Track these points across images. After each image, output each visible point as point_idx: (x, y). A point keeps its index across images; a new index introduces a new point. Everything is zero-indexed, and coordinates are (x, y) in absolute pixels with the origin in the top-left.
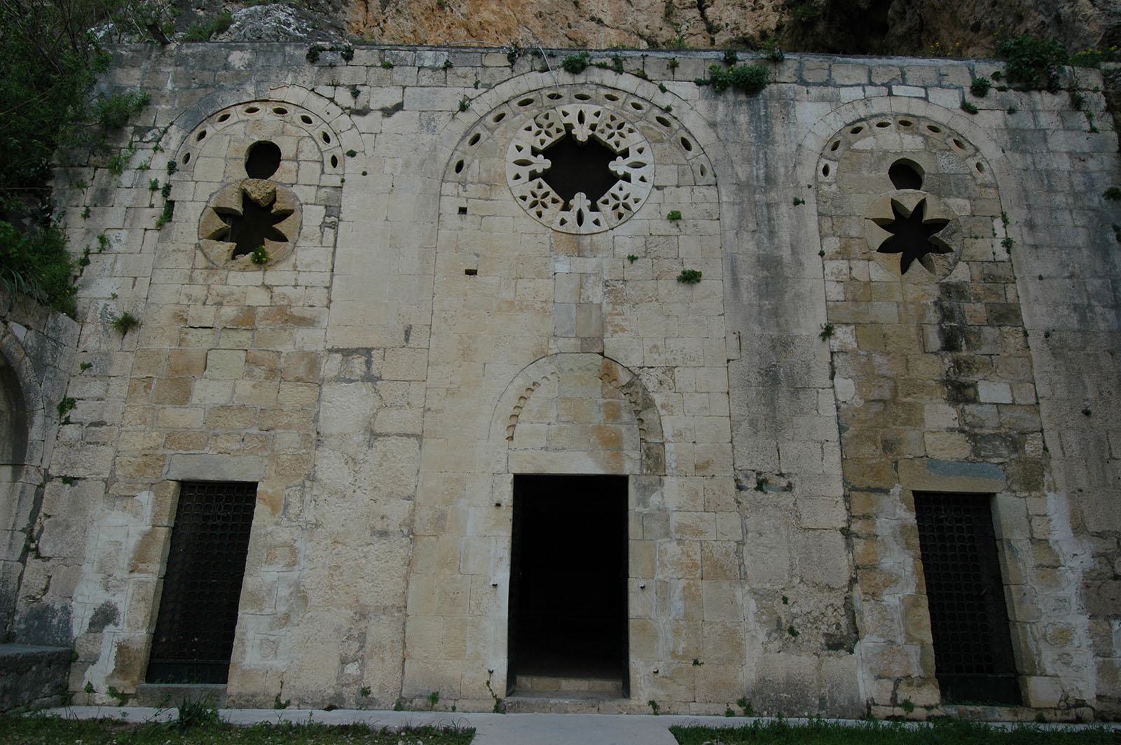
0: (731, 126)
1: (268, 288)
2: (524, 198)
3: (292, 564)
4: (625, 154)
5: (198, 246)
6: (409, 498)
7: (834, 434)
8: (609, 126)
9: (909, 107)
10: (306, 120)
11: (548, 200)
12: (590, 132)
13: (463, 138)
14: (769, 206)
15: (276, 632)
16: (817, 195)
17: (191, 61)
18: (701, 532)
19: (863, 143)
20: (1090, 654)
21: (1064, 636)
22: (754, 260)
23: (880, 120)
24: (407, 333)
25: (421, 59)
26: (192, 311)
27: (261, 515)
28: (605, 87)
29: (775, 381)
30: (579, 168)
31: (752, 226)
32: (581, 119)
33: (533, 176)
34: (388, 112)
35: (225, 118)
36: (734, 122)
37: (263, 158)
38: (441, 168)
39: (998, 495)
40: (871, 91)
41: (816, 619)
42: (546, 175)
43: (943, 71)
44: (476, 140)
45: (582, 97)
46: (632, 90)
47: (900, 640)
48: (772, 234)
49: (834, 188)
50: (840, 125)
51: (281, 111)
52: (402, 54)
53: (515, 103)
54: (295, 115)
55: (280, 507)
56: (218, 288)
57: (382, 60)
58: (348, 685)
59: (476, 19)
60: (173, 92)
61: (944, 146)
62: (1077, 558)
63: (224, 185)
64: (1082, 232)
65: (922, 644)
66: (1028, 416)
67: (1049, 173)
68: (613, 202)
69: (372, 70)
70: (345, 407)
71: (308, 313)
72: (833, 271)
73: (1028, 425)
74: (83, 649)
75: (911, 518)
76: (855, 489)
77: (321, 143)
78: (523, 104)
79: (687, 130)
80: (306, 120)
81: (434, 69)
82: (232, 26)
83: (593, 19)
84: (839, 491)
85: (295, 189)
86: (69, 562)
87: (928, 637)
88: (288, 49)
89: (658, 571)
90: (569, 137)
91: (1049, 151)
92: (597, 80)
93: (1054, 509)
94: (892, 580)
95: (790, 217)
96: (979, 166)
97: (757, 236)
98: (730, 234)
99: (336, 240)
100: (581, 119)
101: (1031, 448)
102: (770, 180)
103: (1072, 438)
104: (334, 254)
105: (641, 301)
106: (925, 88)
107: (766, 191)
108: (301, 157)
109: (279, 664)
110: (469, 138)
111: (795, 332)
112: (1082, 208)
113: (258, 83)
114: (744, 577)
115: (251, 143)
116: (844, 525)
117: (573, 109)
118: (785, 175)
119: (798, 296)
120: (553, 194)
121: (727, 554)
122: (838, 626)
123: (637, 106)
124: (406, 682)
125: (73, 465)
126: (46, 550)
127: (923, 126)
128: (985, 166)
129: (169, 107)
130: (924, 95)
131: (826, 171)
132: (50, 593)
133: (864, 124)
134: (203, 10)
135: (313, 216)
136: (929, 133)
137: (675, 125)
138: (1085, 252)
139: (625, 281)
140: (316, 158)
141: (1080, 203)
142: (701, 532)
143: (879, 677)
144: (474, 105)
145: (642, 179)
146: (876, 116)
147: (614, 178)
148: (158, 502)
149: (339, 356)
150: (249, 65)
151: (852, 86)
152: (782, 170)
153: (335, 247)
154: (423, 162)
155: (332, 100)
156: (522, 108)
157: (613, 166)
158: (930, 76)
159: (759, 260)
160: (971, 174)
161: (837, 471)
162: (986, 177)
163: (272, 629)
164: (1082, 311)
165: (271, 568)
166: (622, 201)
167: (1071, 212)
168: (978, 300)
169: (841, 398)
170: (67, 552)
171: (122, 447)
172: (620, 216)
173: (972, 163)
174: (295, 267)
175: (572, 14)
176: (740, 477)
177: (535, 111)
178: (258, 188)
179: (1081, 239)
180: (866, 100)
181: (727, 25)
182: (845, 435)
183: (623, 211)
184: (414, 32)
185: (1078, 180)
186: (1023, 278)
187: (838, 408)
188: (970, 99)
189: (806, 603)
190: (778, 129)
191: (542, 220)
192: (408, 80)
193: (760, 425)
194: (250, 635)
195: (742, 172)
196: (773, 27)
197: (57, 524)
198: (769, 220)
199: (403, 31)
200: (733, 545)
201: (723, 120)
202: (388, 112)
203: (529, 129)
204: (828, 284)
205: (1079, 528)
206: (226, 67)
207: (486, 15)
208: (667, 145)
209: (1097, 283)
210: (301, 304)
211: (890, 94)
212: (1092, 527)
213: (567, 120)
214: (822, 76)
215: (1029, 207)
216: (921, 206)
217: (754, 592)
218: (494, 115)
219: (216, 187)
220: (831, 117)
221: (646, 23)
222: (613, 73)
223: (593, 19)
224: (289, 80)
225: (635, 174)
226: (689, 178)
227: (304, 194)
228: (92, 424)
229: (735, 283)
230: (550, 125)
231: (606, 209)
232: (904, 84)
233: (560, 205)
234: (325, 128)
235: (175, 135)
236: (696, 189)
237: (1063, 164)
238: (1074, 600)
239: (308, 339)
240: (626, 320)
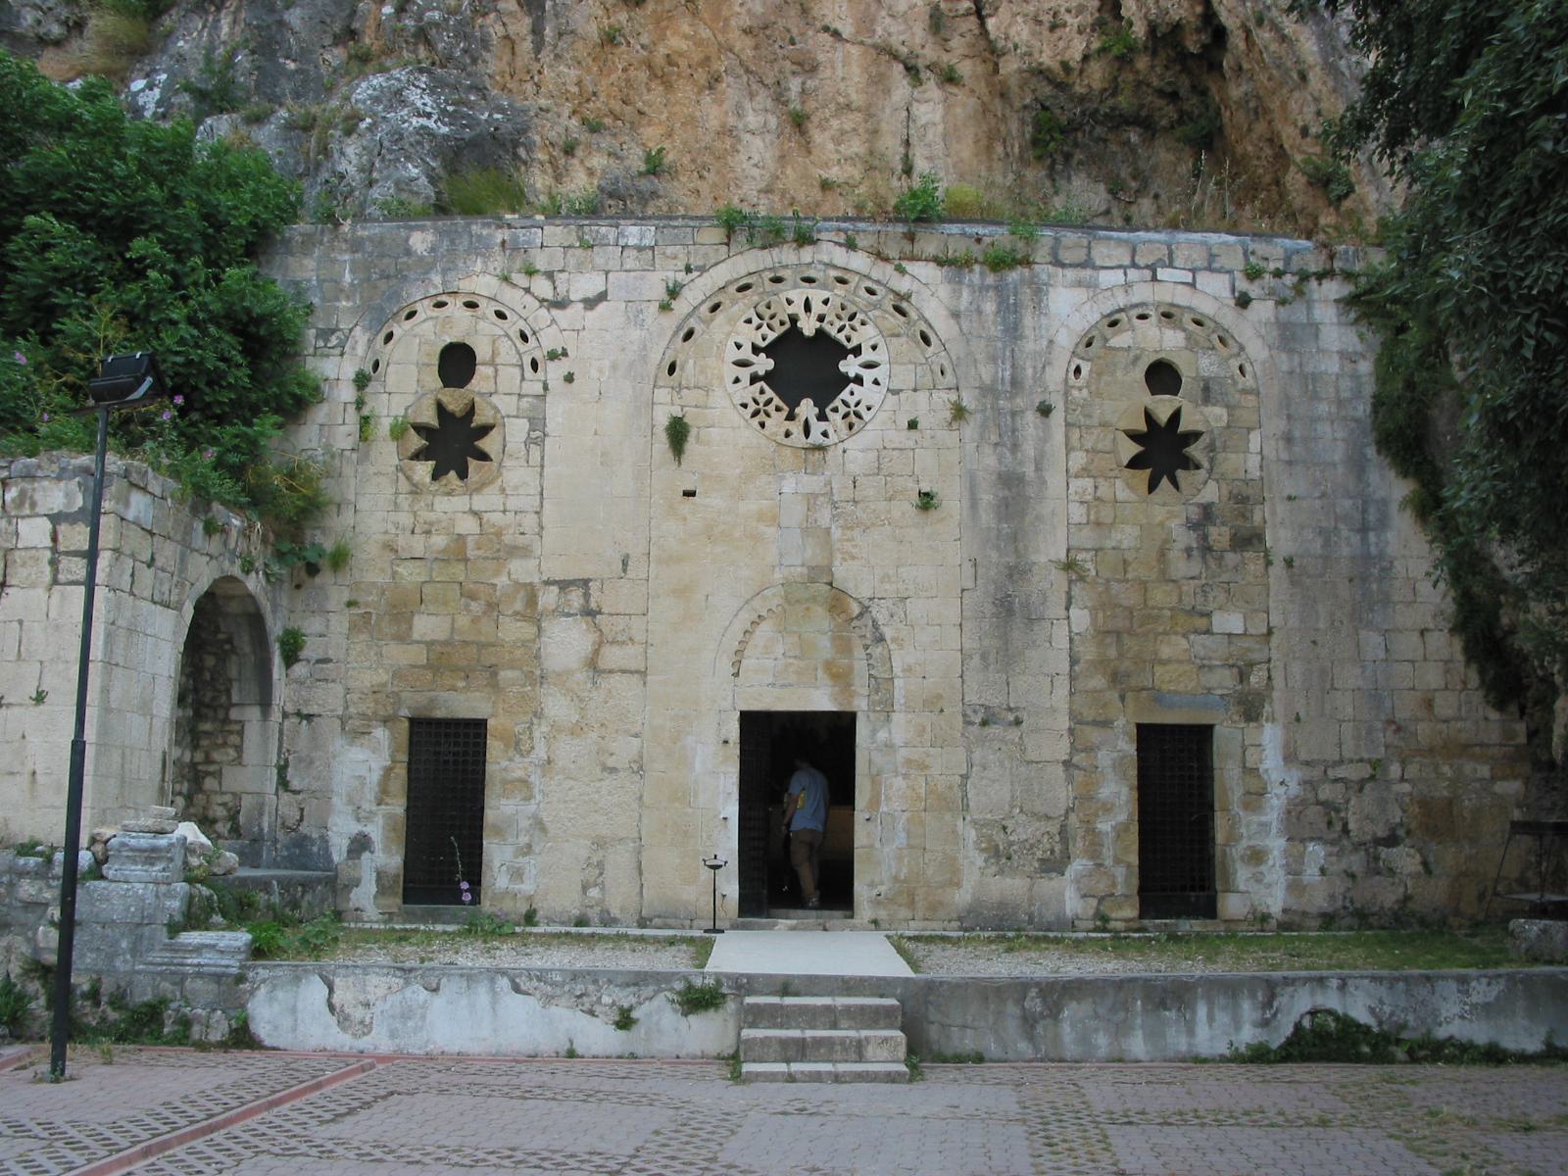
0: (975, 316)
1: (475, 513)
2: (745, 406)
3: (528, 798)
4: (857, 351)
5: (399, 469)
6: (636, 736)
7: (1065, 667)
8: (839, 317)
9: (1174, 295)
10: (501, 315)
11: (771, 408)
12: (818, 325)
13: (676, 333)
14: (1014, 414)
15: (520, 859)
16: (1066, 402)
17: (369, 247)
18: (927, 767)
19: (1120, 340)
20: (1282, 873)
21: (1257, 856)
22: (994, 477)
23: (1140, 311)
24: (625, 564)
25: (624, 236)
26: (401, 542)
27: (494, 748)
28: (835, 267)
29: (1010, 612)
30: (806, 369)
31: (994, 438)
32: (808, 307)
33: (754, 379)
34: (591, 303)
35: (411, 315)
36: (979, 312)
37: (457, 363)
38: (652, 369)
39: (1217, 729)
40: (1133, 274)
41: (1032, 846)
42: (768, 378)
43: (1215, 251)
44: (689, 335)
45: (809, 280)
46: (866, 271)
47: (1108, 862)
48: (1015, 447)
49: (1085, 392)
50: (1097, 317)
51: (471, 305)
52: (603, 230)
53: (732, 289)
54: (487, 309)
55: (515, 744)
56: (425, 515)
57: (581, 239)
58: (592, 907)
59: (662, 50)
60: (352, 285)
61: (1207, 344)
62: (1282, 783)
63: (420, 398)
64: (1341, 445)
65: (1129, 866)
66: (1257, 646)
67: (1315, 377)
68: (843, 410)
69: (570, 252)
70: (565, 643)
71: (521, 540)
72: (1079, 492)
73: (1256, 656)
74: (345, 874)
75: (1131, 749)
76: (1080, 723)
77: (519, 342)
78: (741, 289)
79: (926, 321)
80: (501, 315)
81: (640, 249)
82: (363, 125)
83: (826, 29)
84: (1064, 723)
85: (494, 399)
86: (319, 795)
87: (1134, 859)
88: (474, 227)
89: (883, 804)
90: (794, 330)
91: (1319, 350)
92: (826, 259)
93: (1270, 737)
94: (1107, 808)
95: (1036, 428)
96: (1241, 369)
97: (999, 448)
98: (970, 447)
99: (542, 458)
100: (808, 307)
101: (1256, 679)
102: (1016, 383)
103: (1297, 669)
104: (541, 475)
105: (873, 524)
106: (1194, 271)
107: (1012, 397)
108: (498, 360)
109: (527, 887)
110: (682, 334)
111: (1033, 558)
112: (1345, 418)
113: (444, 272)
114: (966, 808)
115: (443, 345)
116: (1066, 757)
117: (798, 295)
118: (1034, 378)
119: (1039, 518)
120: (777, 401)
121: (951, 788)
122: (1052, 852)
123: (871, 292)
124: (645, 903)
125: (307, 702)
126: (295, 784)
127: (1187, 318)
128: (1248, 368)
129: (350, 304)
130: (1190, 280)
131: (1078, 371)
132: (305, 823)
133: (1122, 316)
134: (294, 61)
135: (516, 431)
136: (1193, 327)
137: (913, 315)
138: (1340, 469)
139: (855, 502)
140: (514, 361)
141: (1343, 413)
142: (927, 767)
143: (1084, 896)
144: (685, 292)
145: (876, 382)
146: (1136, 306)
147: (844, 380)
148: (393, 738)
149: (555, 589)
150: (433, 249)
151: (1112, 268)
152: (1030, 372)
153: (542, 466)
154: (632, 364)
155: (527, 290)
156: (740, 295)
157: (843, 366)
158: (1199, 258)
159: (1000, 476)
160: (1232, 377)
161: (1064, 706)
162: (1248, 381)
163: (516, 857)
164: (1327, 535)
165: (510, 802)
166: (853, 408)
167: (1332, 422)
168: (1223, 524)
169: (1075, 630)
170: (315, 786)
171: (351, 684)
172: (851, 426)
173: (1235, 364)
174: (503, 490)
175: (792, 21)
176: (969, 712)
177: (756, 298)
178: (455, 401)
179: (1338, 455)
180: (1127, 286)
181: (1016, 47)
182: (1076, 668)
183: (853, 419)
184: (579, 84)
185: (1346, 384)
186: (1272, 499)
187: (1071, 640)
188: (1243, 285)
189: (1024, 830)
190: (1028, 320)
191: (766, 431)
192: (611, 263)
193: (991, 659)
194: (497, 864)
195: (986, 373)
196: (1078, 57)
197: (300, 760)
198: (1014, 431)
199: (564, 84)
200: (958, 779)
201: (967, 309)
202: (591, 303)
203: (749, 321)
204: (1071, 505)
205: (1290, 757)
206: (408, 252)
207: (675, 43)
208: (904, 339)
209: (1348, 503)
210: (511, 531)
211: (1154, 279)
212: (1303, 756)
213: (791, 310)
214: (1080, 255)
215: (1289, 417)
216: (1176, 417)
217: (975, 822)
218: (709, 304)
219: (411, 399)
220: (1087, 307)
221: (902, 38)
222: (844, 249)
223: (826, 29)
224: (479, 266)
225: (868, 375)
226: (928, 381)
227: (505, 404)
228: (319, 661)
229: (974, 504)
230: (772, 317)
231: (836, 418)
232: (1171, 265)
233: (784, 414)
234: (522, 325)
235: (361, 336)
236: (935, 394)
237: (1332, 366)
238: (1275, 824)
239: (521, 570)
240: (855, 546)
